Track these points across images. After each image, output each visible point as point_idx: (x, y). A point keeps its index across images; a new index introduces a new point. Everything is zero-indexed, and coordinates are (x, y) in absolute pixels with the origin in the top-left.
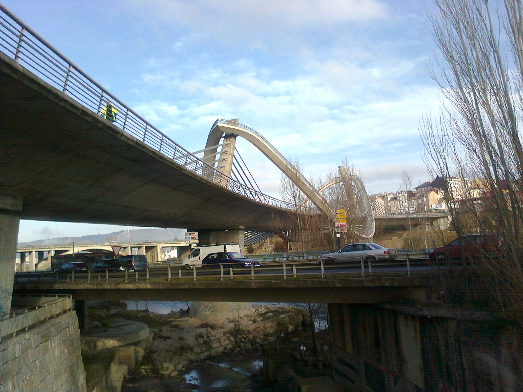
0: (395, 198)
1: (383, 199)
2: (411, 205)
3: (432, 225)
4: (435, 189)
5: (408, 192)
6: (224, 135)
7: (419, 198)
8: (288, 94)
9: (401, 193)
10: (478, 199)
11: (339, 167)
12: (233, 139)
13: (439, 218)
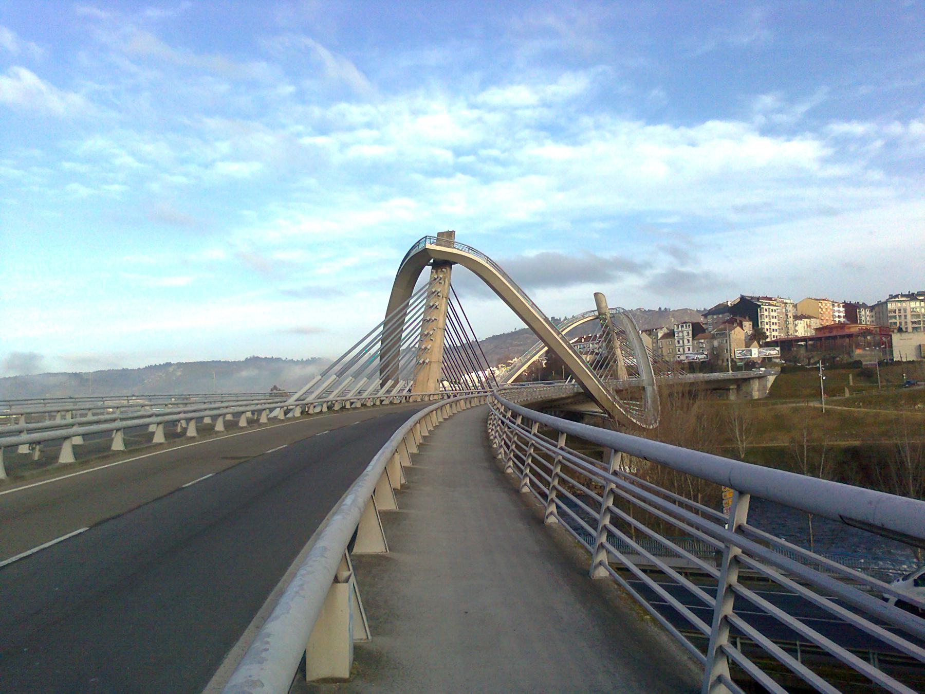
0: (671, 334)
1: (649, 335)
2: (698, 349)
3: (739, 387)
4: (738, 319)
5: (693, 324)
7: (713, 337)
8: (369, 125)
9: (682, 326)
10: (811, 339)
11: (596, 294)
13: (753, 378)
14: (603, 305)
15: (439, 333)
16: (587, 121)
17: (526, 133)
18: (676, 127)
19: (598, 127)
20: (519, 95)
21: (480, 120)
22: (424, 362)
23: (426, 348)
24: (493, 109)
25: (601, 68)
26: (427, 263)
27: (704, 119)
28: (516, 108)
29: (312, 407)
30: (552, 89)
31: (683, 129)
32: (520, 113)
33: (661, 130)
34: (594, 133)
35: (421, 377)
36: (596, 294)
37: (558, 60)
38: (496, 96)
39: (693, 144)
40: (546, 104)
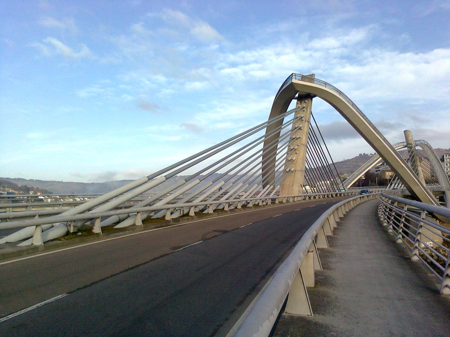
6: (297, 95)
8: (256, 62)
12: (310, 101)
14: (410, 138)
15: (302, 149)
16: (366, 53)
17: (335, 61)
18: (417, 54)
19: (373, 56)
20: (330, 42)
21: (311, 56)
22: (290, 170)
23: (291, 160)
24: (317, 50)
25: (371, 26)
26: (294, 93)
27: (432, 49)
28: (329, 49)
29: (169, 213)
30: (346, 38)
31: (421, 55)
32: (330, 51)
33: (408, 55)
34: (371, 59)
35: (287, 182)
36: (405, 132)
37: (356, 23)
38: (317, 44)
39: (427, 62)
40: (345, 46)
